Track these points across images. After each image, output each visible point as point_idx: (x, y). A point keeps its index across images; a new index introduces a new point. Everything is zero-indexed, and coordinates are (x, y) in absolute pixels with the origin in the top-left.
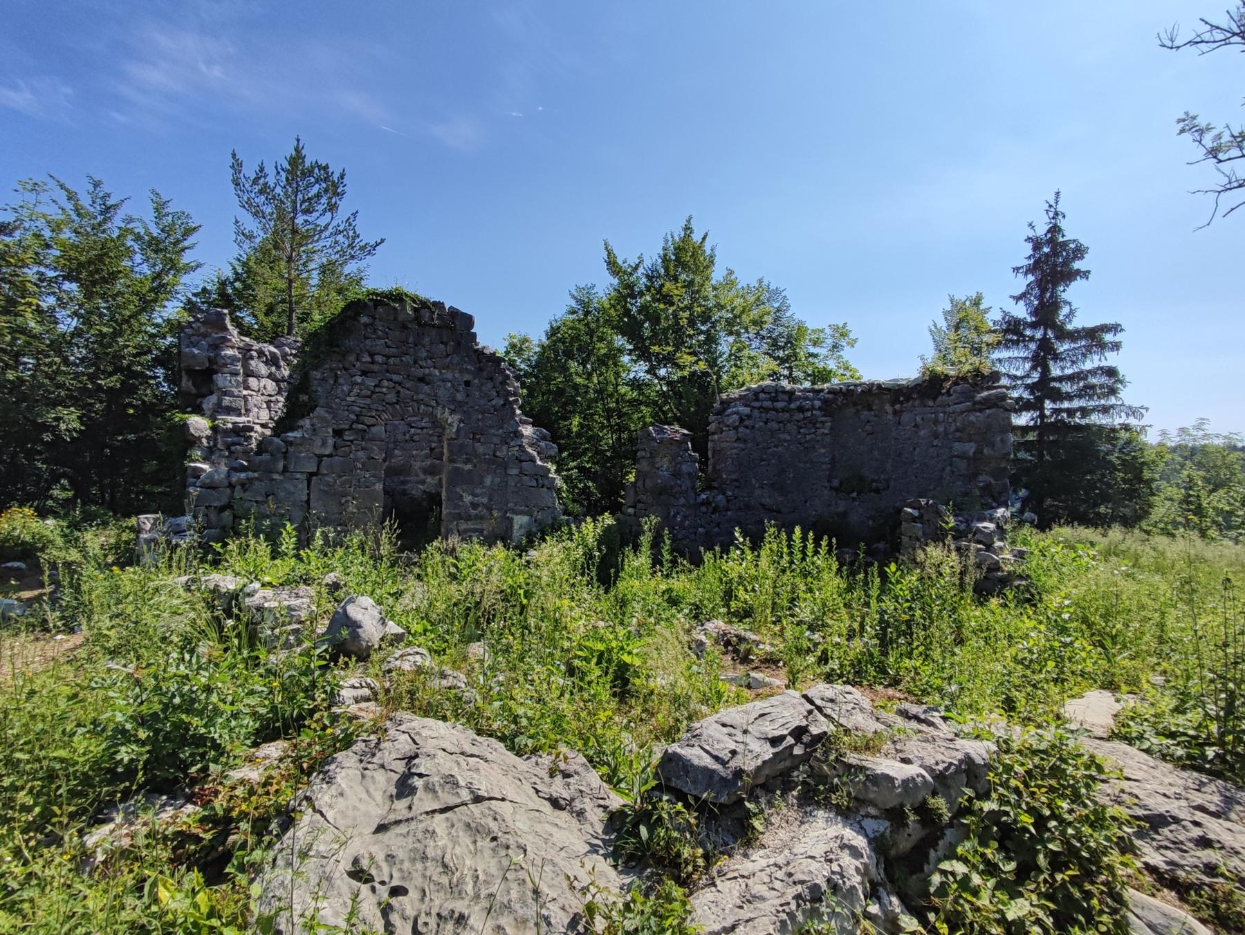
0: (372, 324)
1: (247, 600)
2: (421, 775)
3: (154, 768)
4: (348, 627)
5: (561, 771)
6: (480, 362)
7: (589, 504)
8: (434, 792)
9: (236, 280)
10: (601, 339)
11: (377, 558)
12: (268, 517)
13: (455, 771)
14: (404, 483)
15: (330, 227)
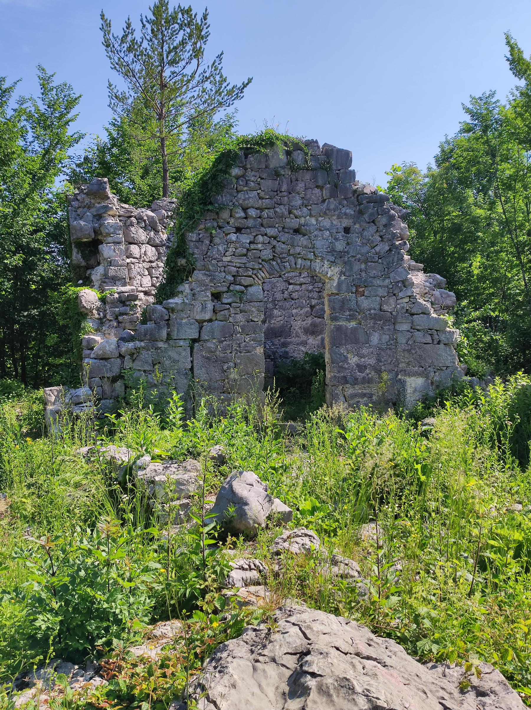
0: (243, 176)
1: (140, 473)
2: (314, 675)
3: (65, 639)
4: (234, 503)
5: (474, 688)
6: (360, 204)
7: (498, 361)
8: (329, 695)
9: (113, 146)
10: (506, 159)
11: (260, 430)
12: (155, 386)
13: (351, 674)
14: (285, 345)
15: (197, 75)
